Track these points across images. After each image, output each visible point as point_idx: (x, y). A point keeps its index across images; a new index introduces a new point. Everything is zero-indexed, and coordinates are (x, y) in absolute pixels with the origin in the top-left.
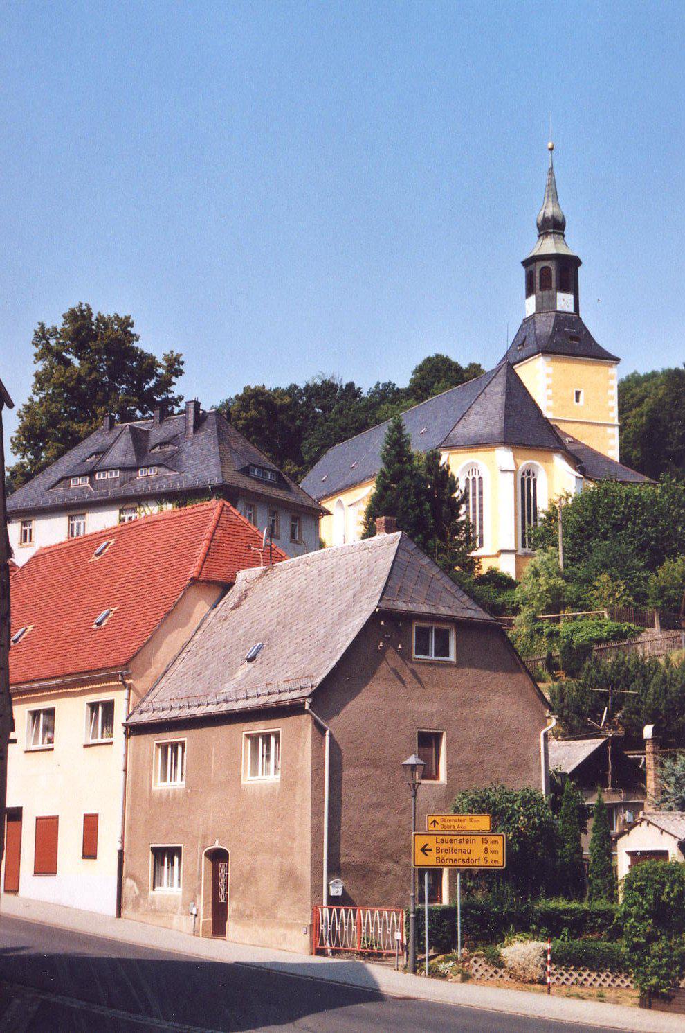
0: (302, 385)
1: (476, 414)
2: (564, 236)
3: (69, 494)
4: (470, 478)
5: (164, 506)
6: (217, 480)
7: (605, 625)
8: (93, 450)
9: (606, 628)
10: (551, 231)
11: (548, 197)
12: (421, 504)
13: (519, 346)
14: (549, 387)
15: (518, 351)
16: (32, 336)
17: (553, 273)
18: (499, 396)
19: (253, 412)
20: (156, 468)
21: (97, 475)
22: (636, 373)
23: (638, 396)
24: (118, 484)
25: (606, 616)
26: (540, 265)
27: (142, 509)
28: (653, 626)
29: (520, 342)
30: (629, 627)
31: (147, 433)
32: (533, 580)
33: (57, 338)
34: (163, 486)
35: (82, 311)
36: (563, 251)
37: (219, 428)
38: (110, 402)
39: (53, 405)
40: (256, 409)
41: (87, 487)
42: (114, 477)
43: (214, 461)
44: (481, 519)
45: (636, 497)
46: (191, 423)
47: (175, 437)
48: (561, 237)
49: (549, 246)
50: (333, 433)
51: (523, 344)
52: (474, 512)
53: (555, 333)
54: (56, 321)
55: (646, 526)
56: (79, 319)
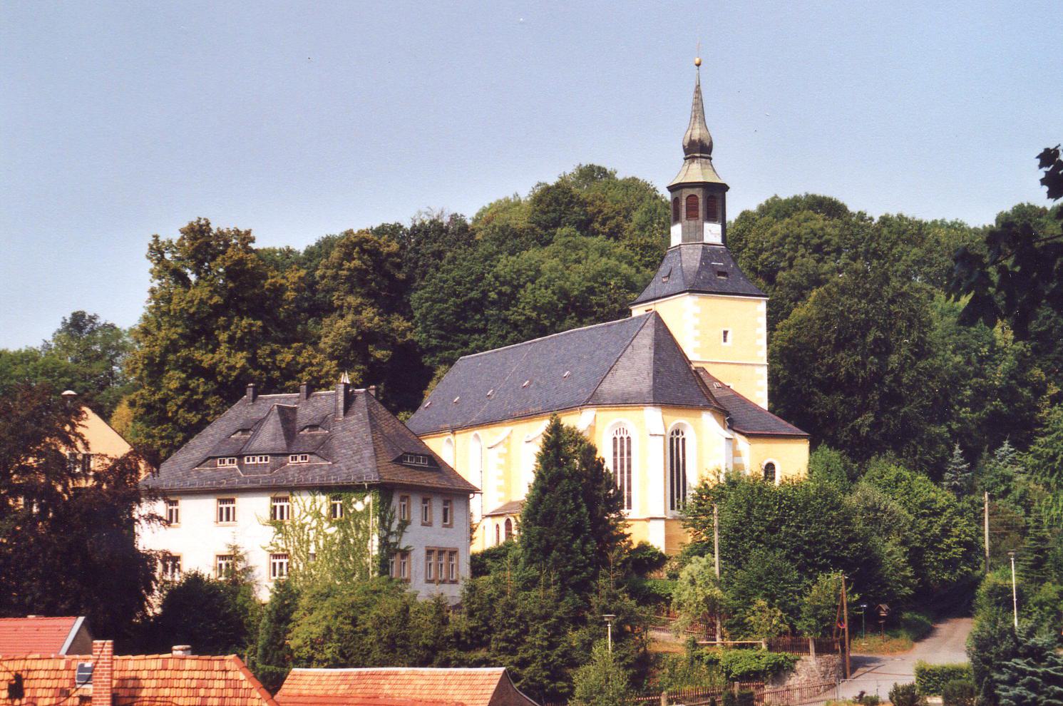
0: (408, 225)
1: (624, 368)
2: (711, 159)
3: (217, 476)
4: (618, 437)
5: (317, 497)
6: (374, 478)
7: (764, 656)
8: (238, 424)
9: (764, 660)
10: (698, 155)
11: (695, 117)
12: (578, 507)
13: (664, 277)
14: (696, 328)
15: (664, 282)
16: (146, 250)
17: (701, 201)
18: (647, 349)
19: (356, 263)
20: (308, 456)
21: (246, 459)
22: (776, 197)
23: (779, 235)
24: (268, 470)
25: (764, 647)
26: (686, 193)
27: (294, 498)
28: (808, 652)
29: (667, 274)
30: (786, 657)
31: (294, 410)
32: (690, 589)
33: (173, 252)
34: (316, 478)
35: (201, 226)
36: (711, 179)
37: (370, 413)
38: (232, 328)
39: (173, 330)
40: (360, 259)
41: (235, 469)
42: (264, 462)
43: (368, 453)
44: (629, 480)
45: (790, 499)
46: (341, 406)
47: (324, 418)
48: (708, 161)
49: (696, 173)
50: (445, 286)
51: (669, 276)
52: (622, 472)
53: (701, 267)
54: (172, 234)
55: (799, 528)
56: (198, 232)
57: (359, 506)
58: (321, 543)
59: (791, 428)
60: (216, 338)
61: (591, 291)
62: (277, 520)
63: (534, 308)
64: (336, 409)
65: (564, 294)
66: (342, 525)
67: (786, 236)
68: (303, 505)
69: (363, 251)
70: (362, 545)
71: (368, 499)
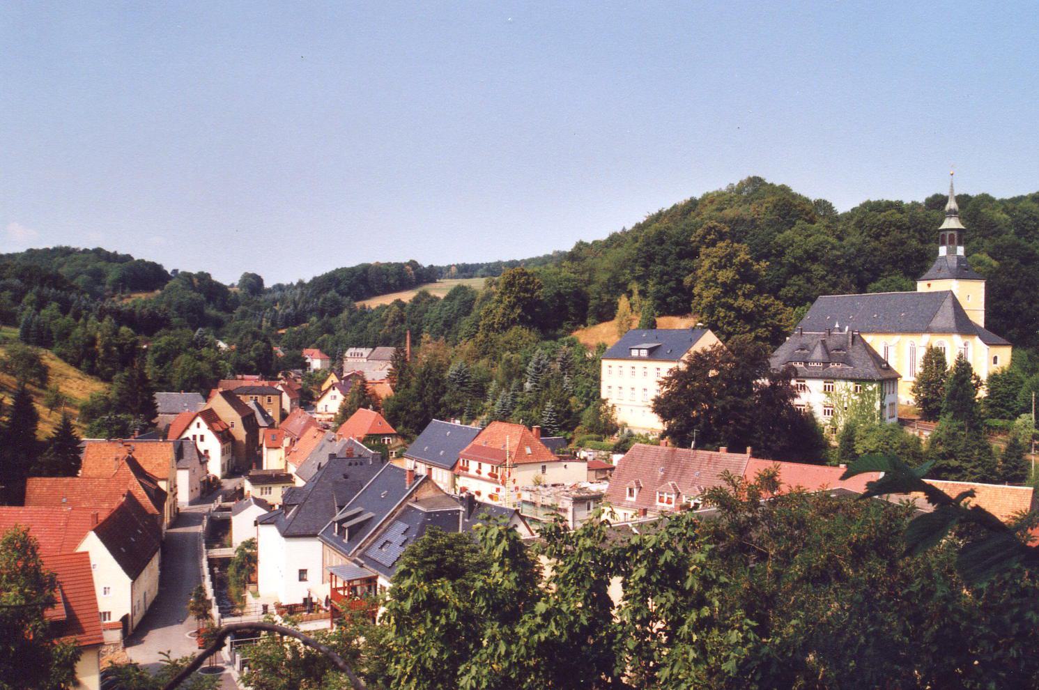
46: (850, 341)
57: (870, 388)
58: (850, 403)
59: (1003, 341)
60: (737, 294)
61: (817, 250)
62: (827, 391)
63: (793, 257)
64: (847, 343)
65: (806, 252)
66: (861, 396)
67: (885, 221)
68: (840, 386)
69: (715, 231)
70: (871, 406)
71: (874, 385)
